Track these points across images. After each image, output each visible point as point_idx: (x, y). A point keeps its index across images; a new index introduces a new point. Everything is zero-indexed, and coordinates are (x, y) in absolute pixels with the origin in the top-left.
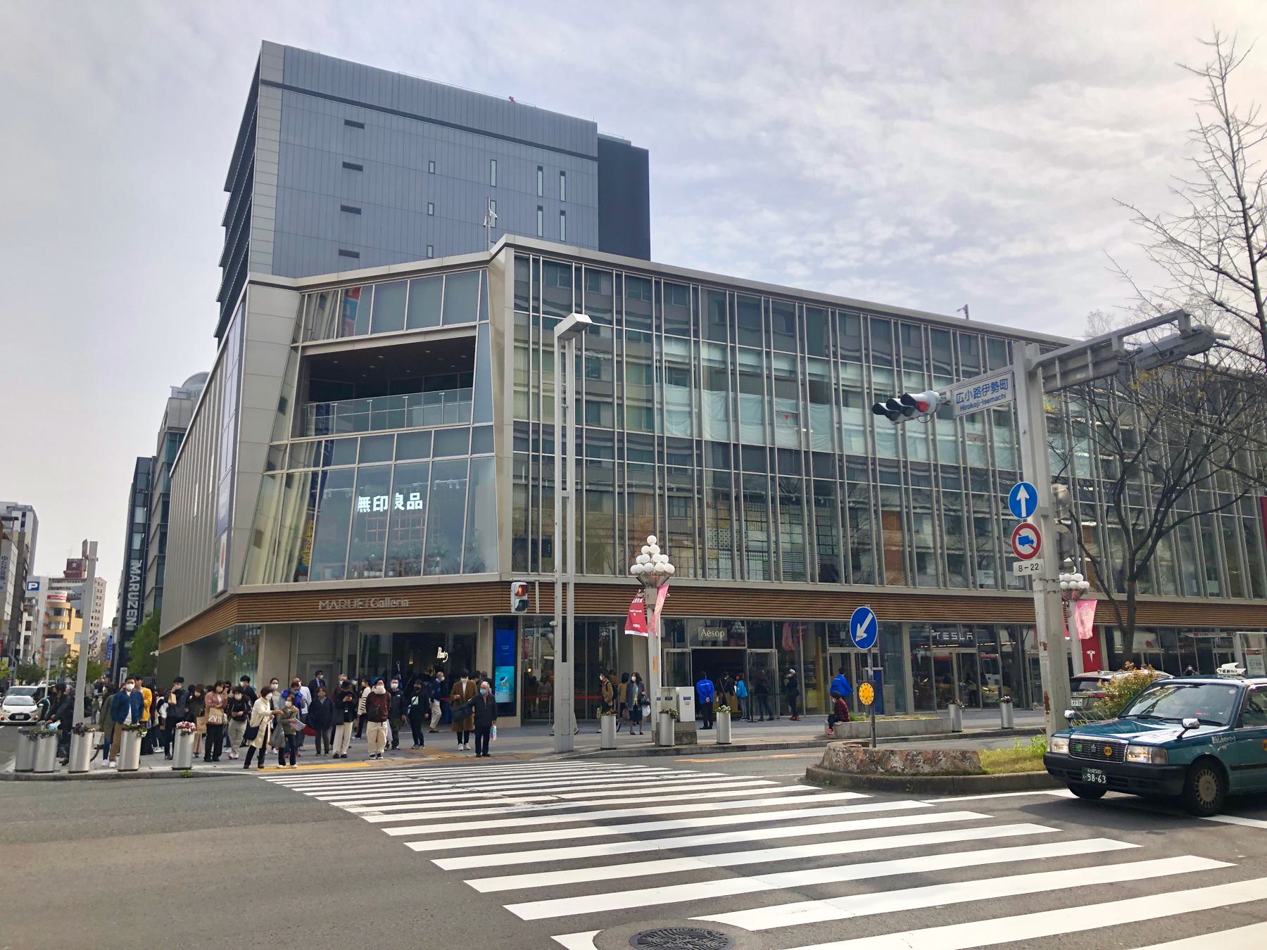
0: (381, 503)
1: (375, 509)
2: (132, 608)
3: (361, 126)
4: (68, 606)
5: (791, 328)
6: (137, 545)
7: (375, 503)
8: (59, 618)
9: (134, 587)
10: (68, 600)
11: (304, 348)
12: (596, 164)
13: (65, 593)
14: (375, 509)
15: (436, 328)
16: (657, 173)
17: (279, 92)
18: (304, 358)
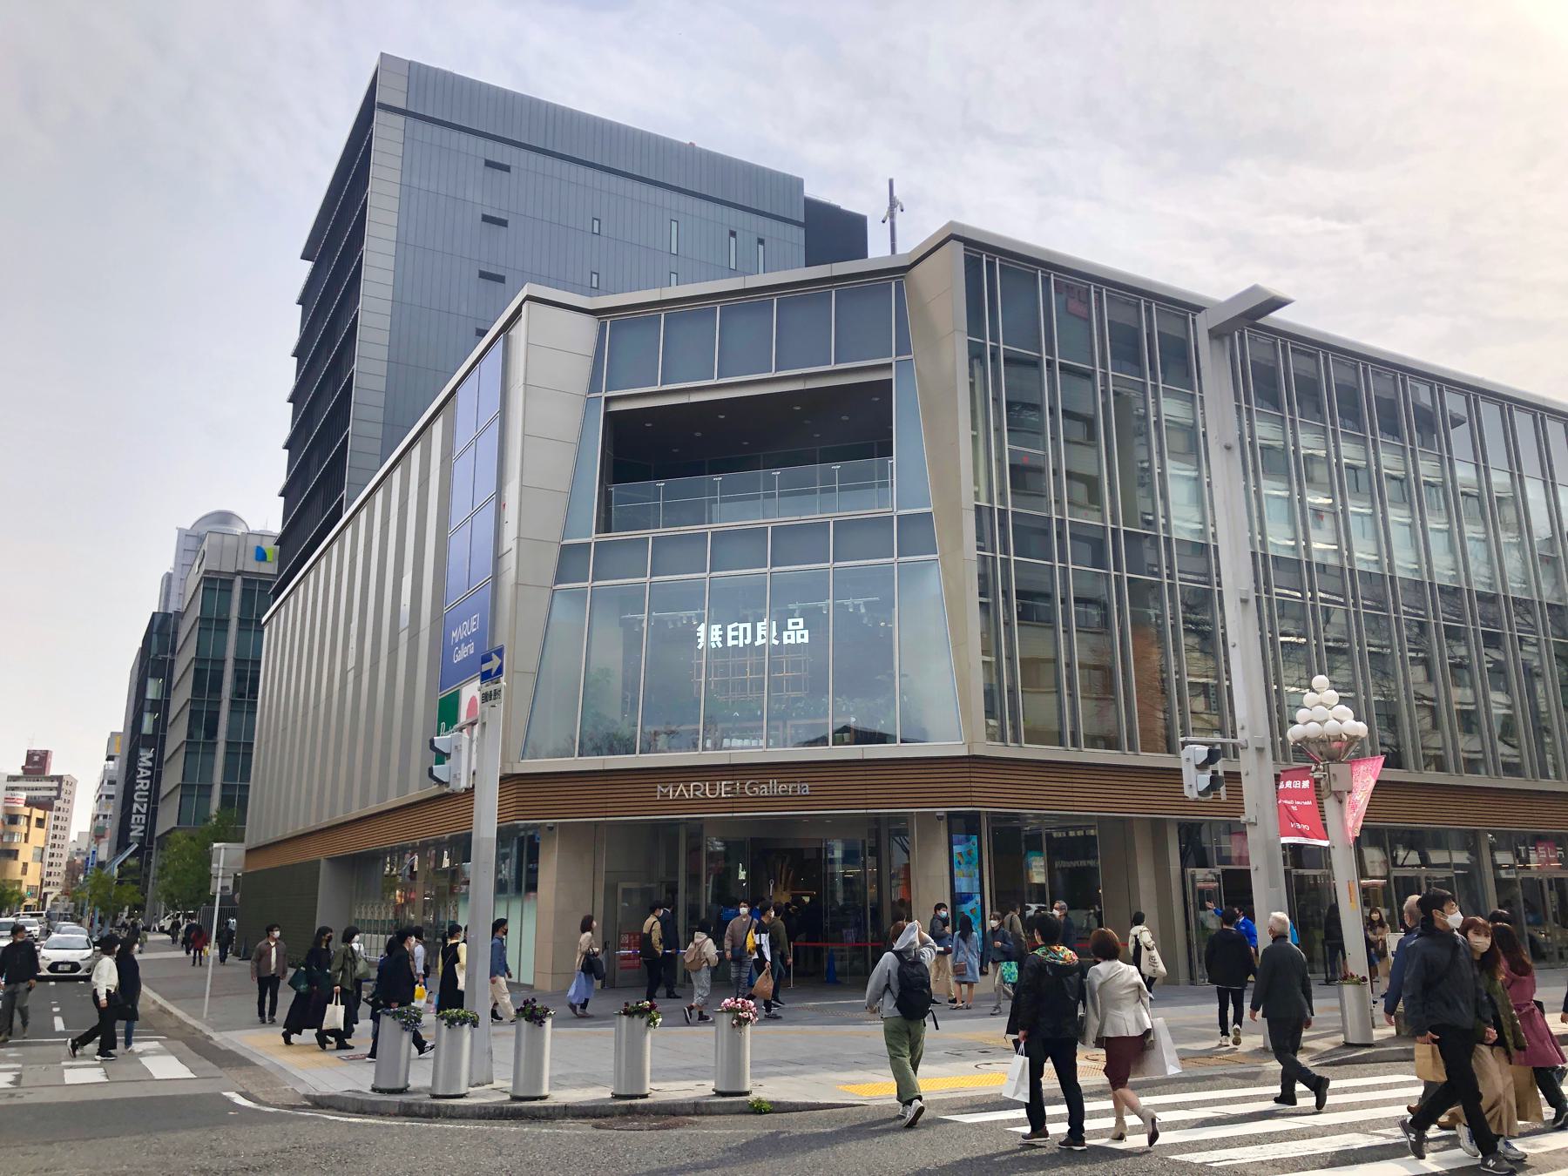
0: (739, 634)
1: (730, 643)
2: (139, 812)
3: (507, 169)
4: (27, 811)
5: (1092, 435)
6: (147, 726)
7: (730, 634)
8: (14, 828)
9: (142, 785)
10: (28, 803)
11: (608, 400)
12: (802, 232)
13: (23, 795)
14: (730, 643)
15: (828, 369)
16: (957, 220)
17: (400, 119)
18: (609, 416)
